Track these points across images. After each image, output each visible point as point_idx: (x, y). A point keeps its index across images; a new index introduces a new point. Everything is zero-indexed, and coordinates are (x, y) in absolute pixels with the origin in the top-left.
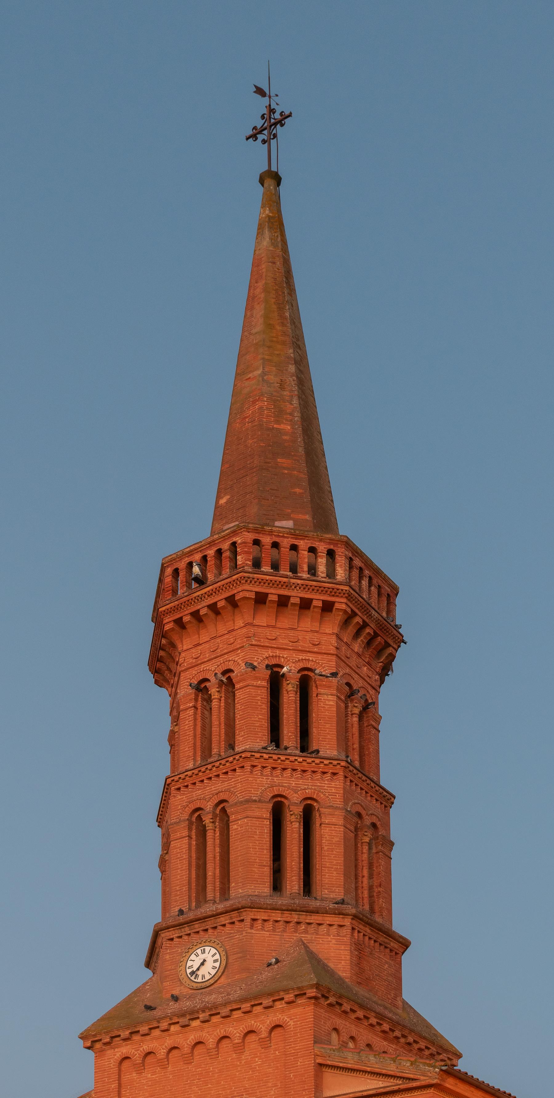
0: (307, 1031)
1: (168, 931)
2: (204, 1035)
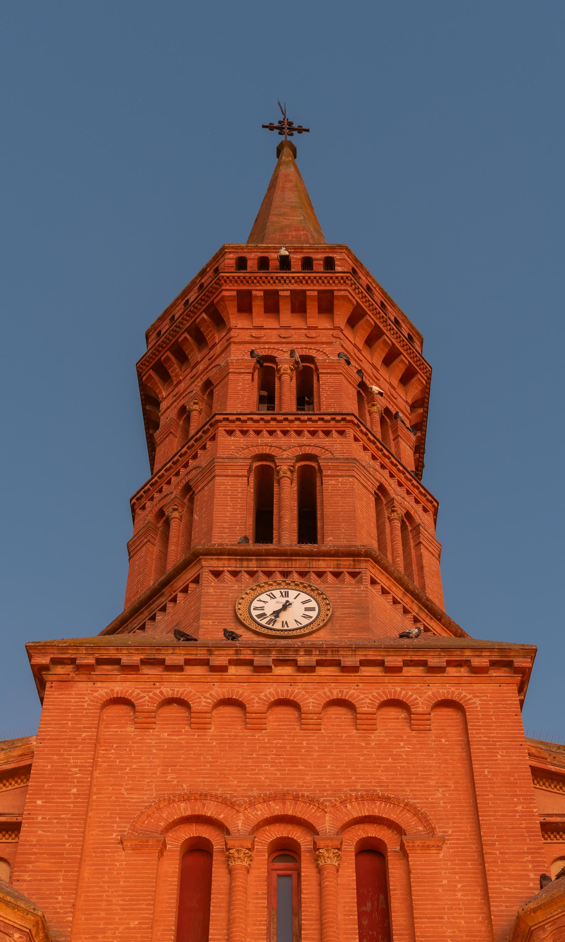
0: (510, 715)
1: (218, 559)
2: (296, 691)
